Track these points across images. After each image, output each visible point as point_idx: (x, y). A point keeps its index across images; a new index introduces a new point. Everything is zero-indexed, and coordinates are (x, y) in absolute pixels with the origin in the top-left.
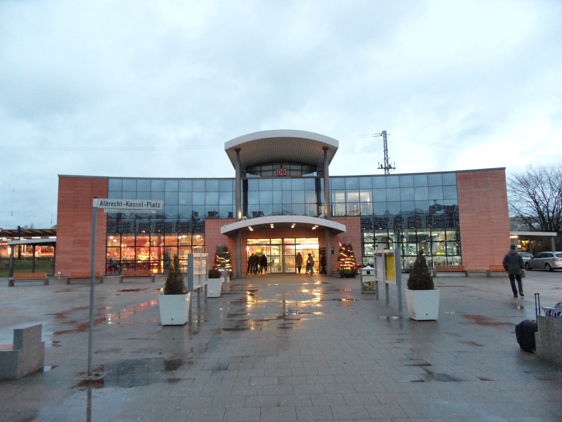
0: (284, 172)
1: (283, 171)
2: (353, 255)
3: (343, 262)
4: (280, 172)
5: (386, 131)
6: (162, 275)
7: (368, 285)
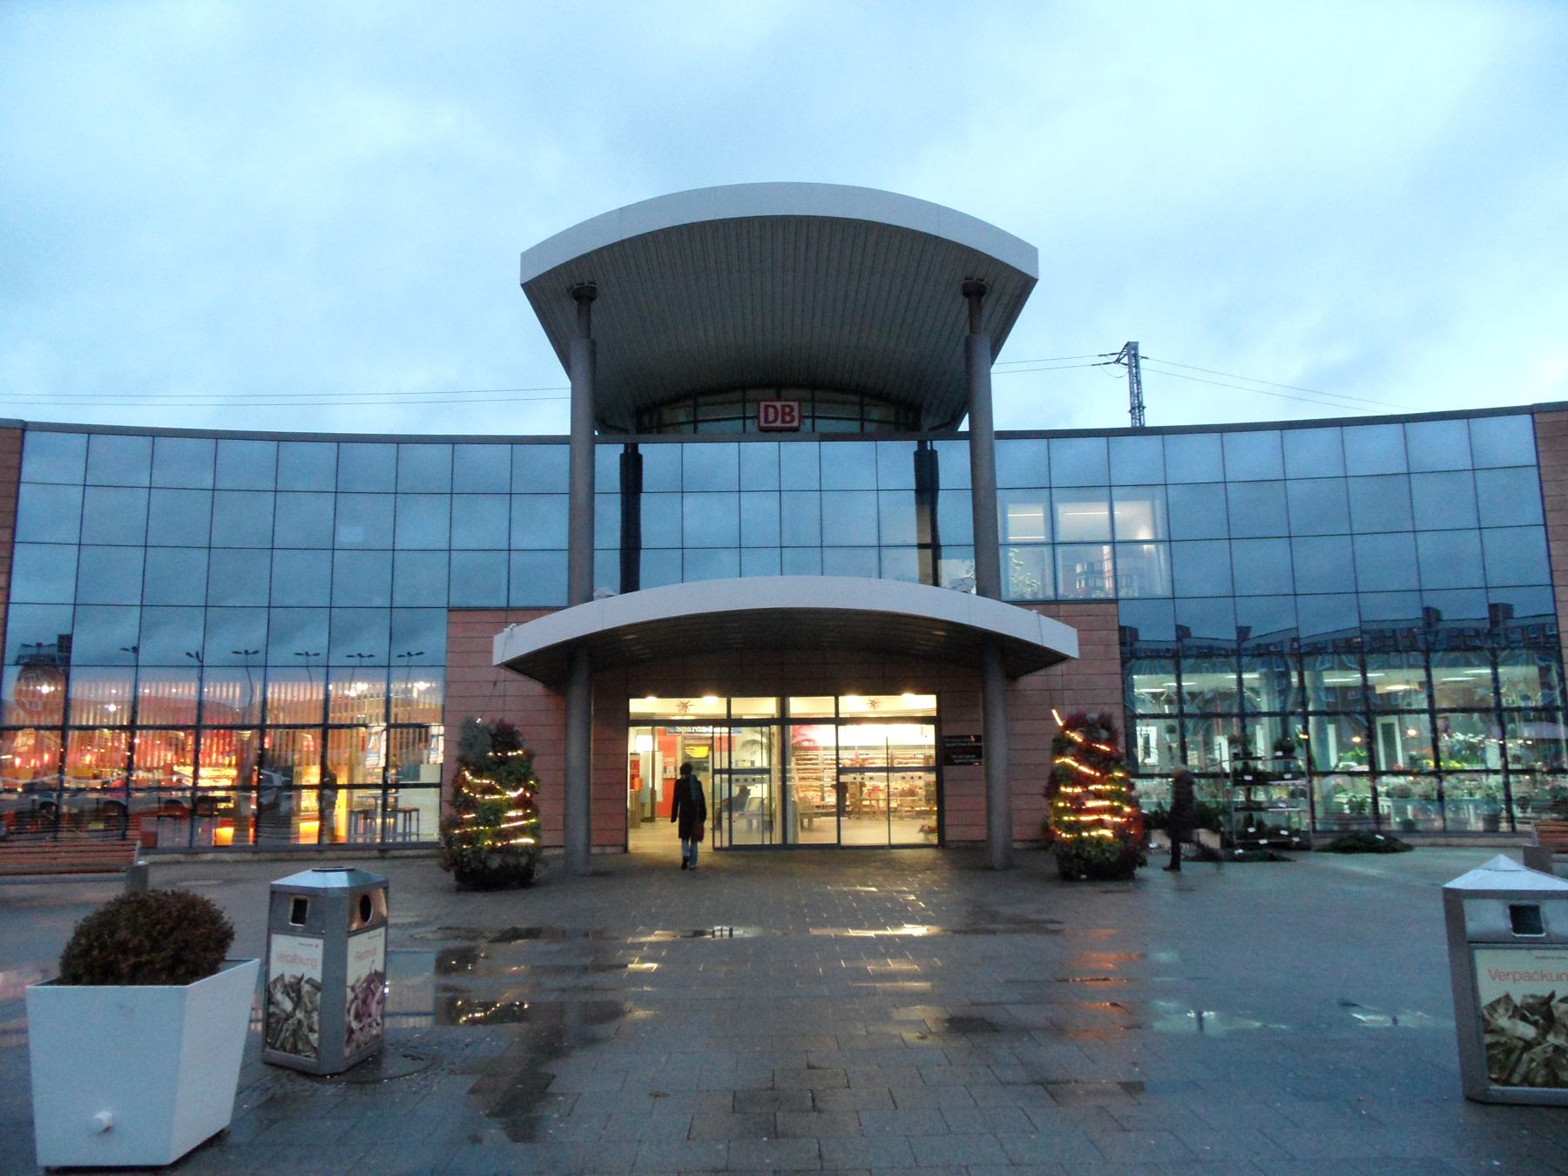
0: (790, 414)
1: (787, 410)
2: (1122, 769)
3: (1075, 799)
4: (771, 411)
5: (1137, 343)
6: (249, 856)
7: (1529, 1031)
